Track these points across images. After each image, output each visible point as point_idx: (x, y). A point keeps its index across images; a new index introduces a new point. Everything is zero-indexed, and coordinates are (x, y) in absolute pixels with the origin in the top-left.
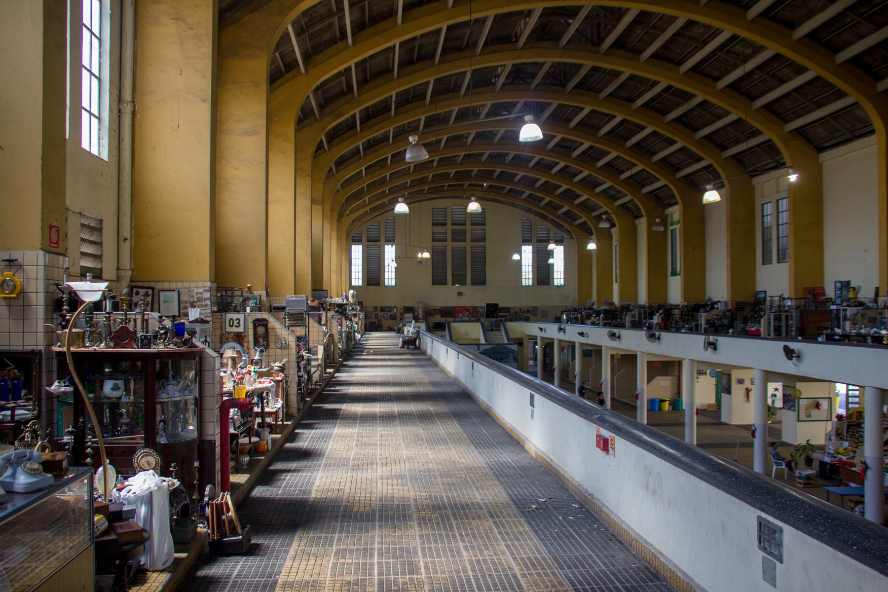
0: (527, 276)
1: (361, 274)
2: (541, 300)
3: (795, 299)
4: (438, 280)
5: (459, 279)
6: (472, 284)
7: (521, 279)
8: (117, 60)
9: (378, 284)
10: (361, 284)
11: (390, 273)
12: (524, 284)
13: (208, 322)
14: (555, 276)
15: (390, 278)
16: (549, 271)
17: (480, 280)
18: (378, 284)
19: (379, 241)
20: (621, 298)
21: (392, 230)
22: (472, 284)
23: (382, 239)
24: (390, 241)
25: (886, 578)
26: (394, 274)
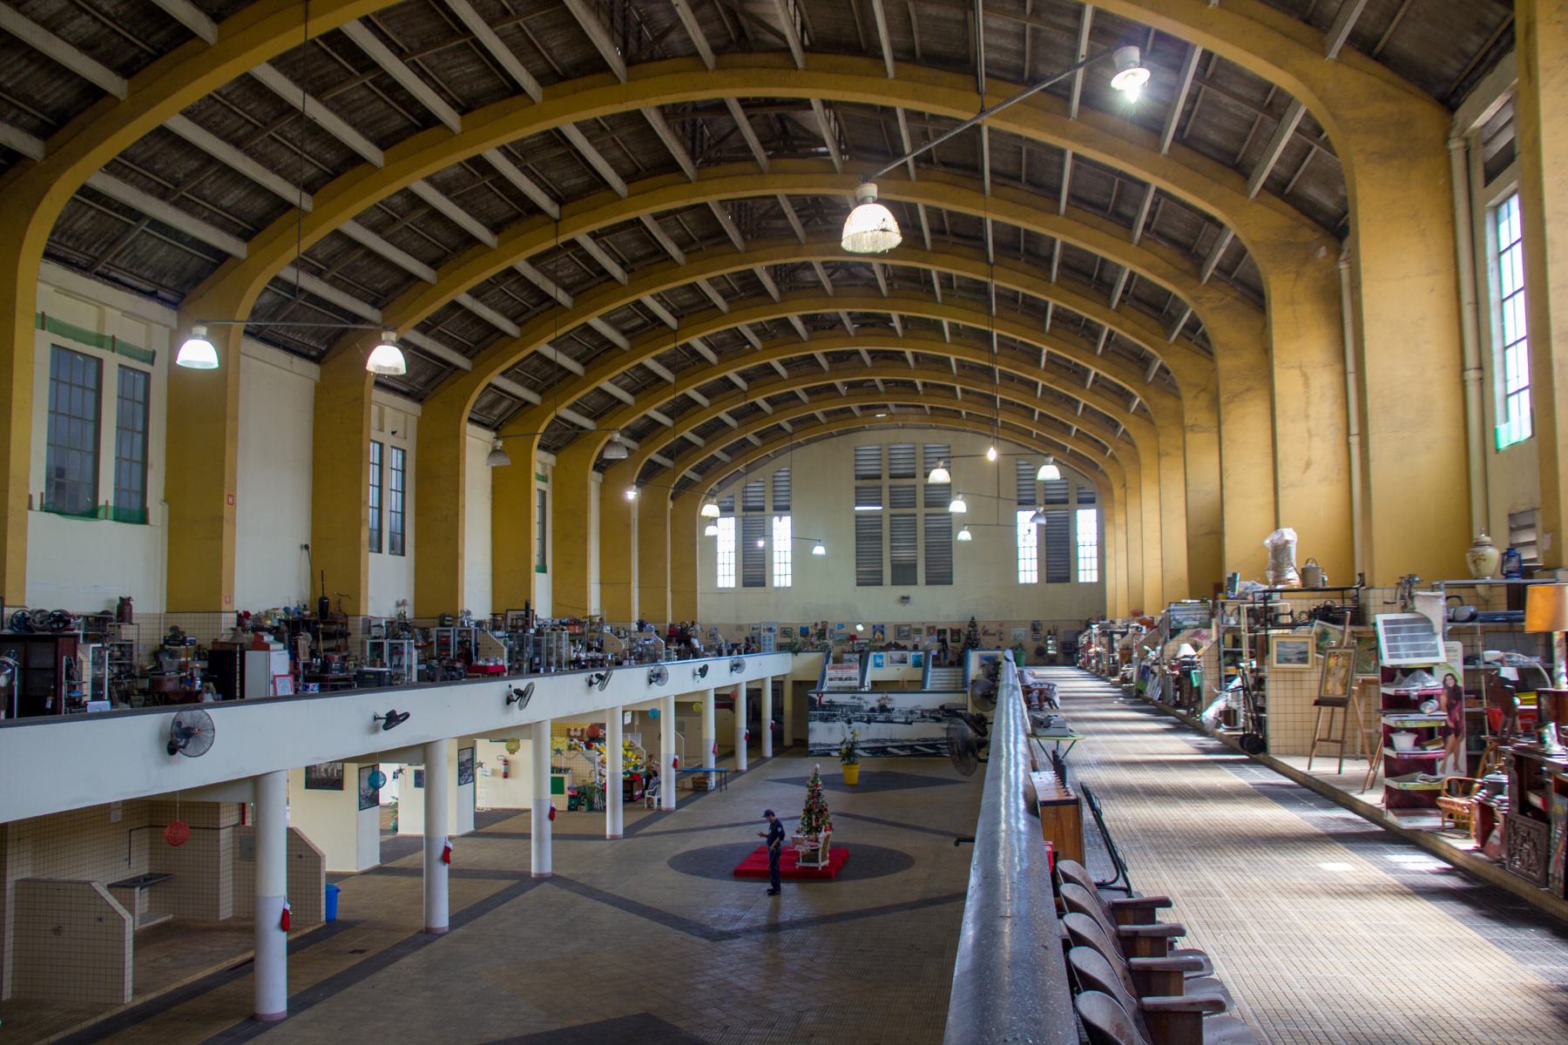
0: (1028, 570)
1: (1035, 563)
2: (755, 611)
3: (221, 612)
4: (869, 578)
5: (904, 574)
6: (928, 583)
7: (1017, 572)
8: (1478, 252)
9: (763, 584)
10: (1035, 580)
11: (1028, 561)
12: (720, 585)
13: (191, 828)
14: (1081, 566)
15: (782, 574)
16: (1069, 565)
17: (941, 576)
18: (763, 584)
19: (762, 509)
20: (556, 604)
21: (777, 499)
22: (928, 583)
23: (1073, 499)
24: (782, 509)
25: (1561, 951)
26: (789, 566)
